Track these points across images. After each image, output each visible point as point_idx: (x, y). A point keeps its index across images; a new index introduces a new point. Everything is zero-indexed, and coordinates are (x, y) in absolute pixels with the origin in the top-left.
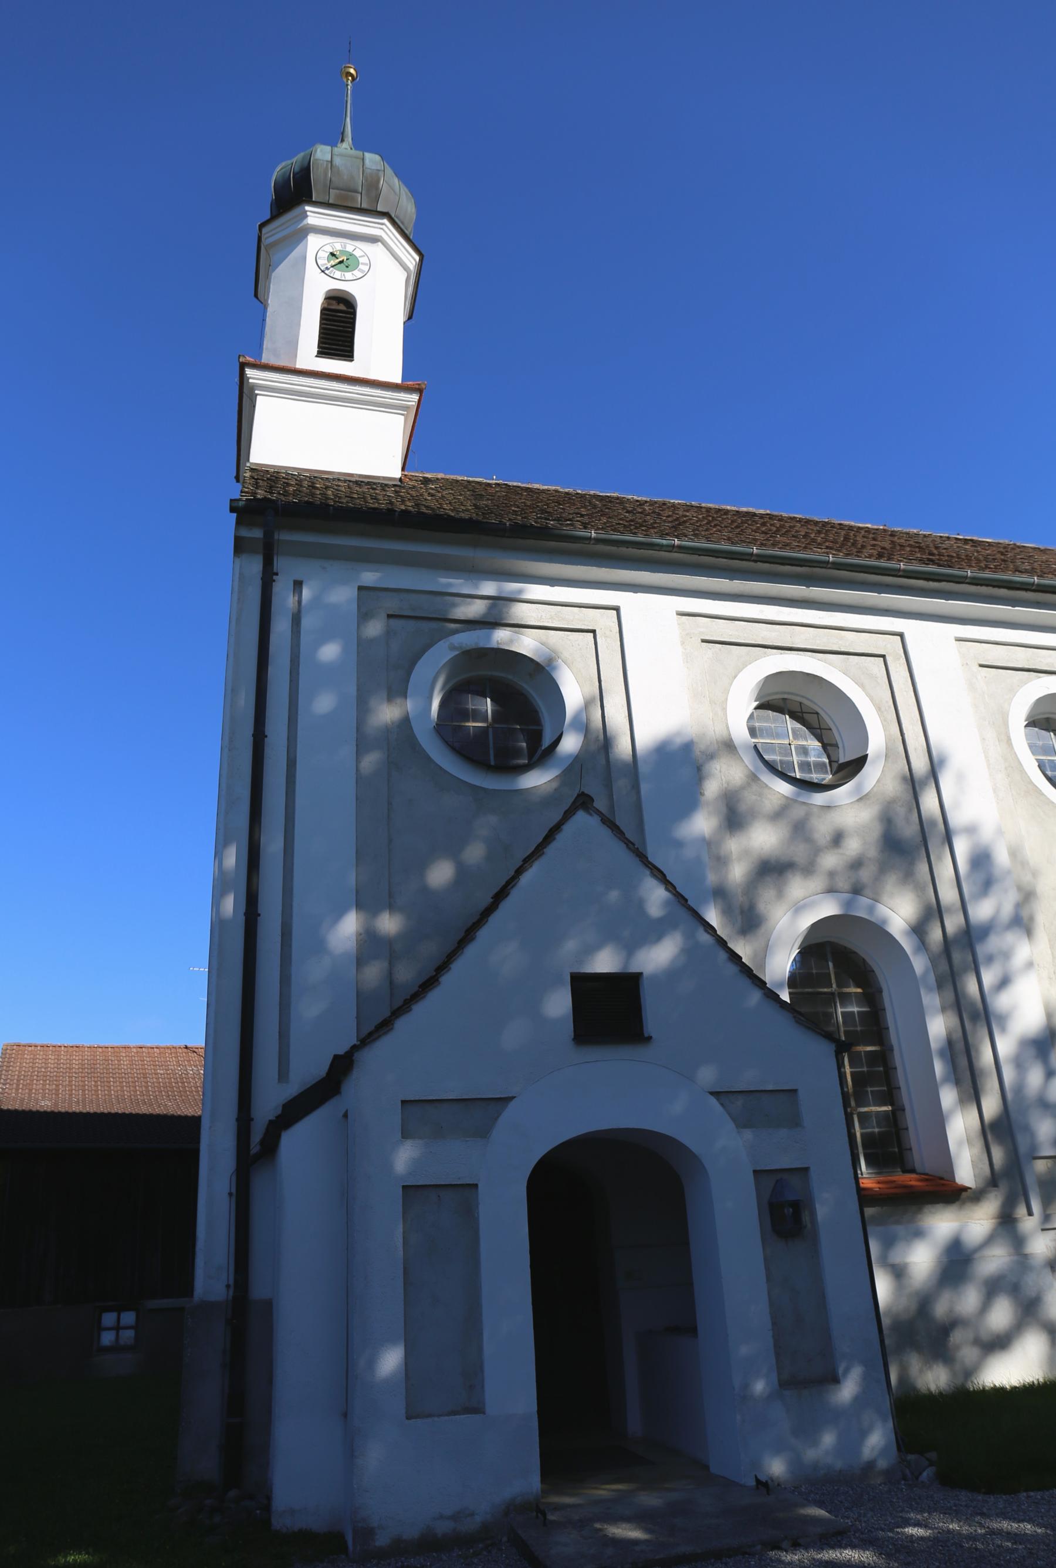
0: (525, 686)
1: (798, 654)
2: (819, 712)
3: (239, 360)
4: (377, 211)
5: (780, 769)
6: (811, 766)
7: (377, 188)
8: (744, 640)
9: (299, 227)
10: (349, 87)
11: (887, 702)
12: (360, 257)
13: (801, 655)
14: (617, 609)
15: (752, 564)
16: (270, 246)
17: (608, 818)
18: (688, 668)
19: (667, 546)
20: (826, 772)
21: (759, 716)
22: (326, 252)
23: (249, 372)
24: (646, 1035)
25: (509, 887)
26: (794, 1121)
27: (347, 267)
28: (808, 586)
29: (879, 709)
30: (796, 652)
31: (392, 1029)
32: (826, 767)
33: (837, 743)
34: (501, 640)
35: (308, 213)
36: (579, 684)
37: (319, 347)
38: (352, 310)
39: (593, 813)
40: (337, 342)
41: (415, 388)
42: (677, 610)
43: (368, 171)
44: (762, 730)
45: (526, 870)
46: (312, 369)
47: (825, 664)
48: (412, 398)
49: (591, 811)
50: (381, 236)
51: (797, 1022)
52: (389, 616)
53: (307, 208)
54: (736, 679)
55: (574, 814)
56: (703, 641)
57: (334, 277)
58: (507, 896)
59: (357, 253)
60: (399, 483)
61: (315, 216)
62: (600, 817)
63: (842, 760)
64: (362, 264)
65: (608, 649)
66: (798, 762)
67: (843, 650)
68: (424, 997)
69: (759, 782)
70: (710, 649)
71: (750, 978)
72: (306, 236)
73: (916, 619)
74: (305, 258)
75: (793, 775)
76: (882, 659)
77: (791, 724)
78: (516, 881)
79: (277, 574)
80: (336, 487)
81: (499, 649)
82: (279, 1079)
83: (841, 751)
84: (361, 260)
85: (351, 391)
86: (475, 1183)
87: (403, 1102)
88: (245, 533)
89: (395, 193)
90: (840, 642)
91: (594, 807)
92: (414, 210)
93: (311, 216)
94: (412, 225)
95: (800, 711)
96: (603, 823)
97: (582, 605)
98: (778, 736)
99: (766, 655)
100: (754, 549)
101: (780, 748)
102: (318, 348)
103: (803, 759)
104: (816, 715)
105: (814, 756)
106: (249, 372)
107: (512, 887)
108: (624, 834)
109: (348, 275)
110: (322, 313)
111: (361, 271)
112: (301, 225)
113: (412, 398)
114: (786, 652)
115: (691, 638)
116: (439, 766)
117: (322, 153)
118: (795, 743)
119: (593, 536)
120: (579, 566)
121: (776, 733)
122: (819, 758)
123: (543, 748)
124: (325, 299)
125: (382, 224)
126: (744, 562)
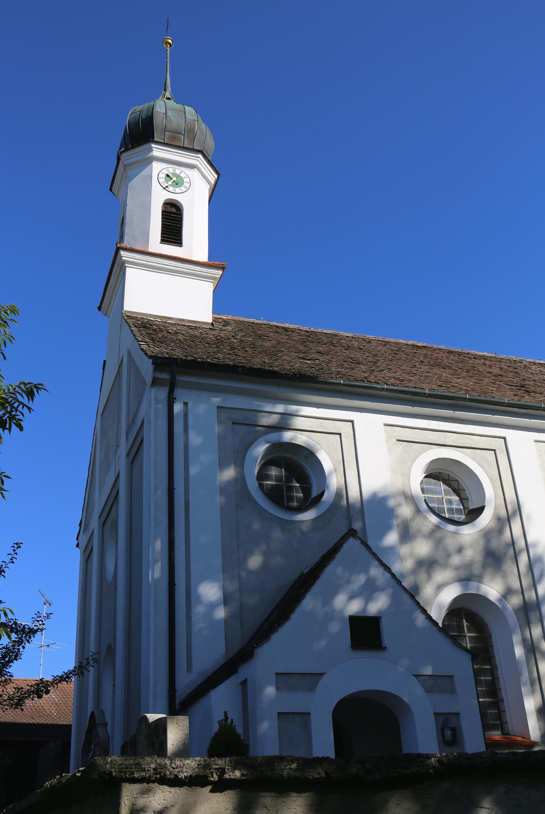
0: (303, 463)
1: (448, 448)
2: (458, 480)
3: (117, 246)
4: (194, 149)
5: (437, 512)
6: (454, 511)
7: (194, 132)
8: (419, 440)
9: (147, 156)
10: (168, 52)
11: (496, 476)
12: (180, 174)
13: (449, 449)
14: (352, 422)
15: (424, 398)
16: (125, 166)
17: (364, 542)
18: (389, 455)
19: (381, 388)
20: (462, 514)
21: (426, 482)
22: (164, 174)
23: (122, 253)
24: (383, 646)
25: (320, 574)
26: (452, 690)
27: (177, 184)
28: (454, 411)
29: (491, 480)
30: (447, 447)
31: (270, 639)
32: (462, 511)
33: (468, 498)
34: (292, 438)
35: (153, 149)
36: (332, 463)
37: (162, 237)
38: (180, 213)
39: (357, 539)
40: (172, 234)
41: (221, 267)
42: (384, 423)
43: (188, 121)
44: (428, 490)
45: (327, 566)
46: (160, 253)
47: (463, 454)
48: (218, 273)
49: (356, 538)
50: (197, 165)
51: (453, 643)
52: (234, 423)
53: (153, 145)
54: (415, 462)
55: (348, 539)
56: (398, 440)
57: (169, 190)
58: (319, 578)
59: (183, 175)
60: (212, 327)
61: (157, 151)
62: (360, 540)
63: (470, 508)
64: (186, 182)
65: (348, 445)
66: (447, 508)
67: (472, 446)
68: (284, 625)
69: (427, 519)
70: (401, 445)
71: (431, 621)
72: (151, 162)
73: (513, 429)
74: (151, 177)
75: (443, 515)
76: (494, 452)
77: (443, 487)
78: (323, 571)
79: (175, 399)
80: (170, 324)
81: (291, 443)
82: (187, 670)
83: (470, 502)
84: (185, 180)
85: (181, 266)
86: (309, 712)
87: (276, 674)
88: (159, 375)
89: (203, 134)
90: (471, 442)
91: (358, 536)
92: (213, 143)
93: (155, 151)
94: (212, 154)
95: (448, 479)
96: (362, 544)
97: (334, 419)
98: (436, 493)
99: (431, 449)
100: (427, 391)
101: (437, 500)
102: (161, 237)
103: (450, 506)
104: (457, 482)
105: (456, 505)
106: (122, 253)
107: (321, 574)
108: (372, 549)
109: (178, 190)
110: (162, 215)
111: (185, 187)
112: (149, 156)
113: (218, 273)
114: (442, 447)
115: (391, 438)
116: (262, 507)
117: (160, 106)
118: (445, 497)
119: (342, 383)
120: (333, 398)
121: (435, 491)
122: (458, 506)
123: (312, 497)
124: (163, 204)
125: (198, 157)
126: (420, 397)
